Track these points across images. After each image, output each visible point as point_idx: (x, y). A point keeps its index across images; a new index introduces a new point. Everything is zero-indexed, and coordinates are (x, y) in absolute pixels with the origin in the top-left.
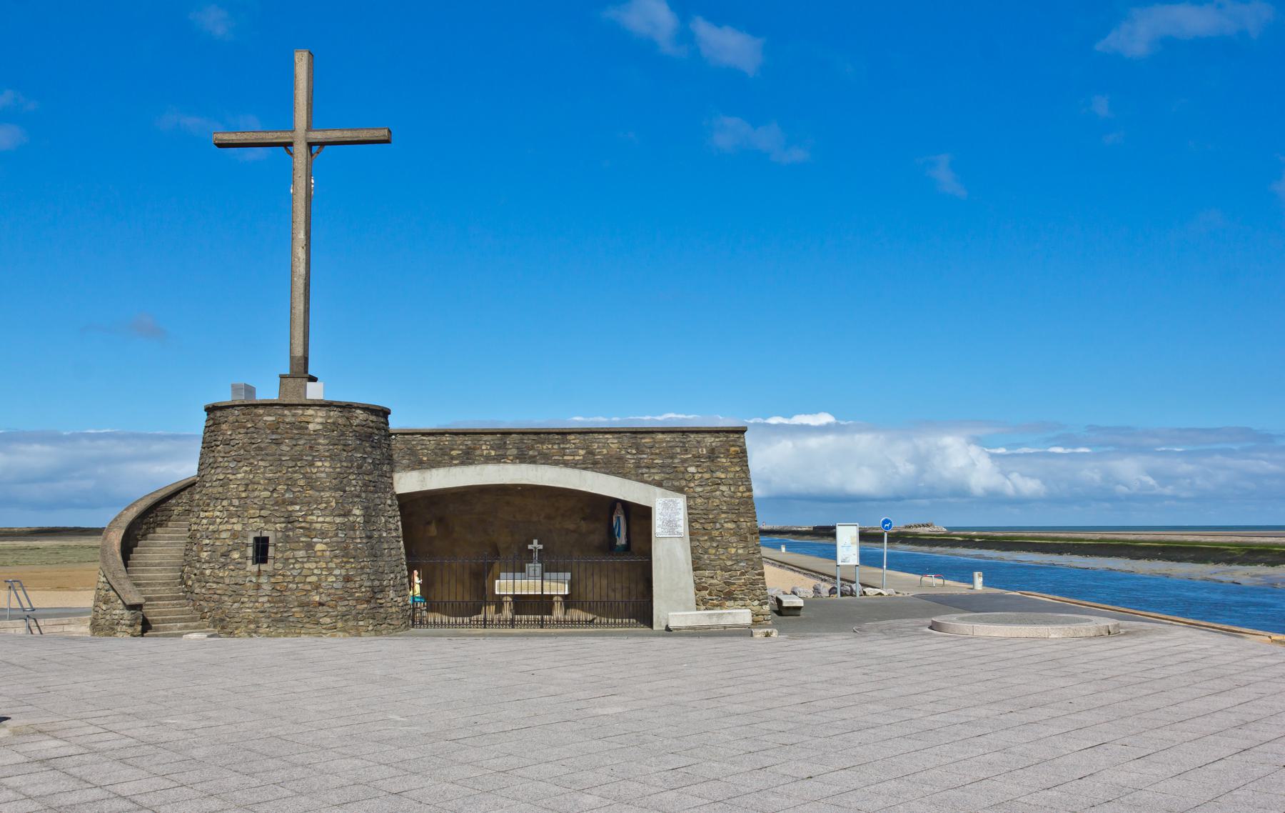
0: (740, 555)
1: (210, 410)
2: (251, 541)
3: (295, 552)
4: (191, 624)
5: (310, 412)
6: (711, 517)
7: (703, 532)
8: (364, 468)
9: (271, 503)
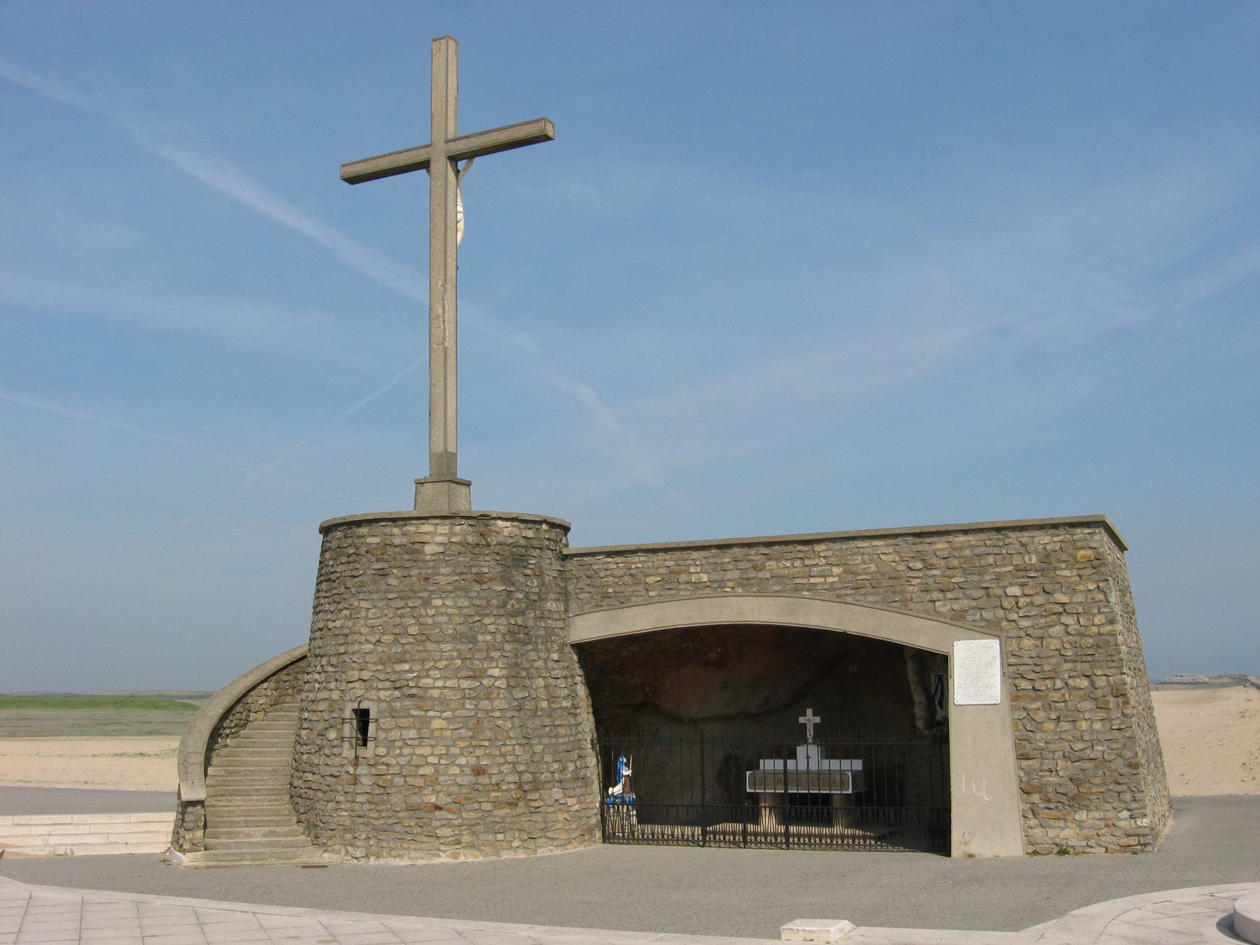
0: (1098, 732)
1: (326, 530)
2: (348, 713)
3: (403, 732)
4: (279, 829)
5: (427, 528)
6: (1046, 668)
7: (1033, 694)
8: (509, 606)
9: (373, 661)
